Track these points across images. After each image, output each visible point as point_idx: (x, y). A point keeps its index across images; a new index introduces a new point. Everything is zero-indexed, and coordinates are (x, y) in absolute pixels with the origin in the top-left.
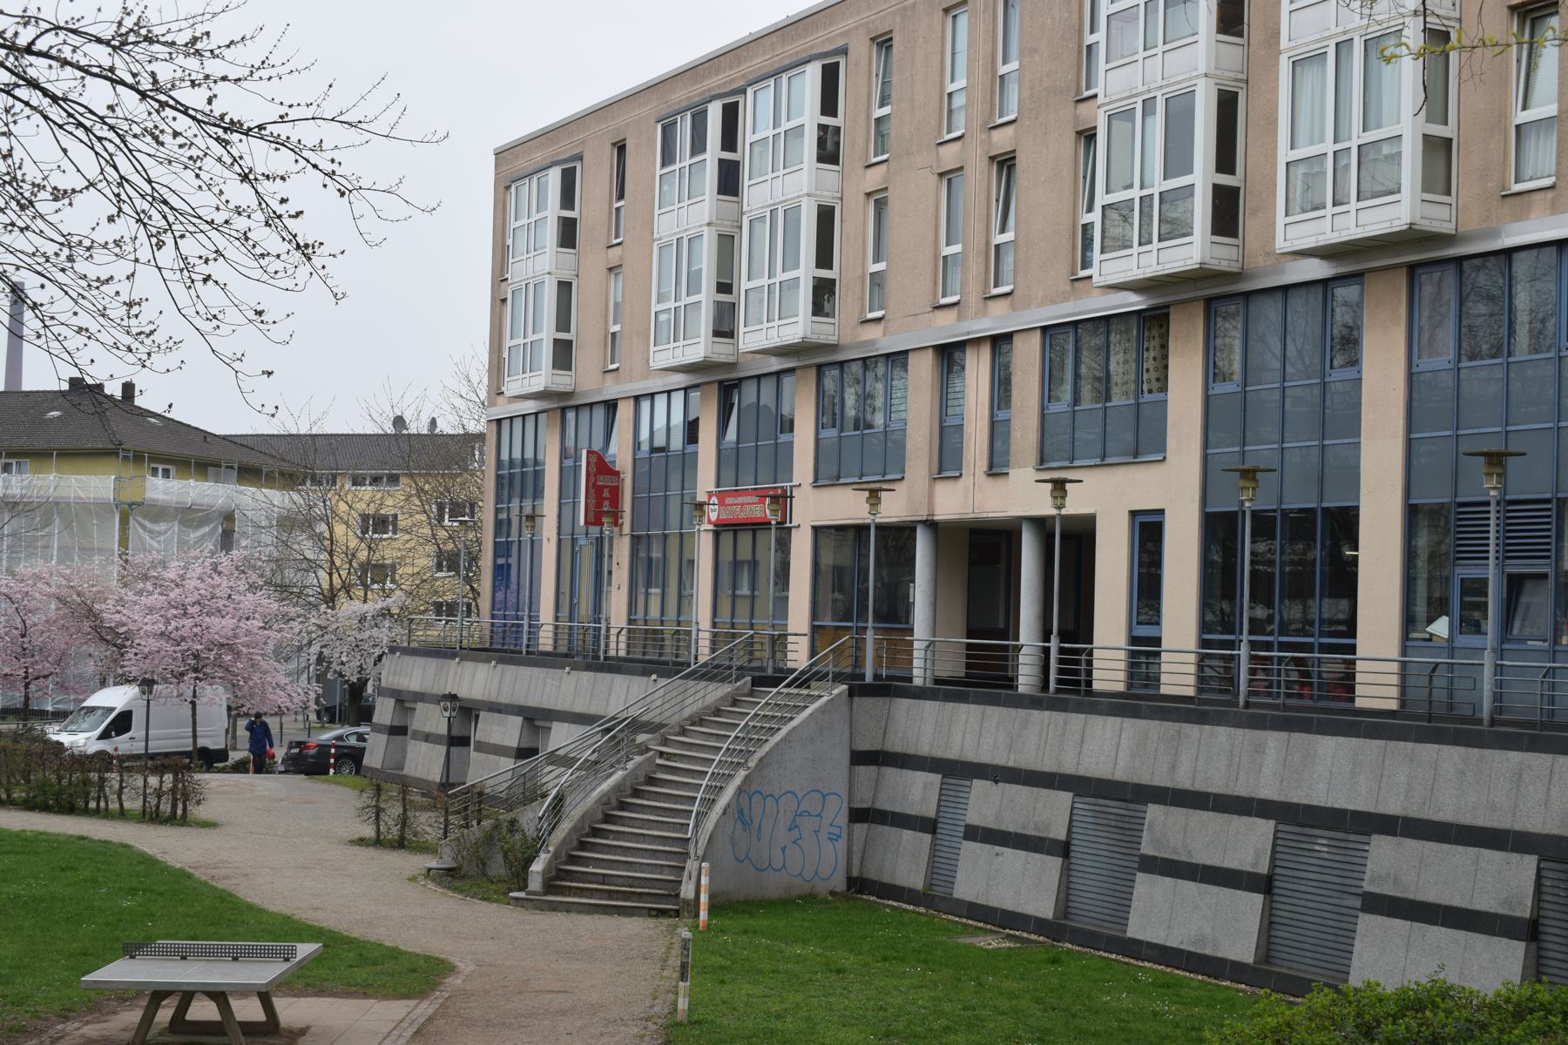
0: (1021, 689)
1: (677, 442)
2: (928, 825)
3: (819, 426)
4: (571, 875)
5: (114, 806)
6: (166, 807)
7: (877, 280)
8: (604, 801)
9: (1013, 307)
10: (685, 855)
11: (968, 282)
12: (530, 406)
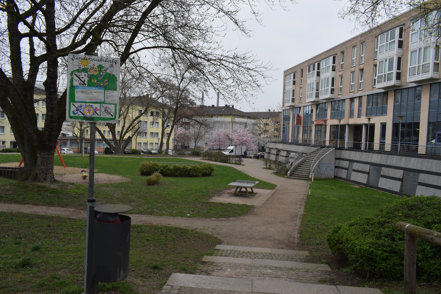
0: (362, 149)
1: (310, 113)
2: (347, 169)
3: (331, 110)
4: (293, 174)
5: (231, 162)
6: (238, 162)
7: (341, 88)
8: (298, 164)
10: (310, 172)
12: (288, 108)
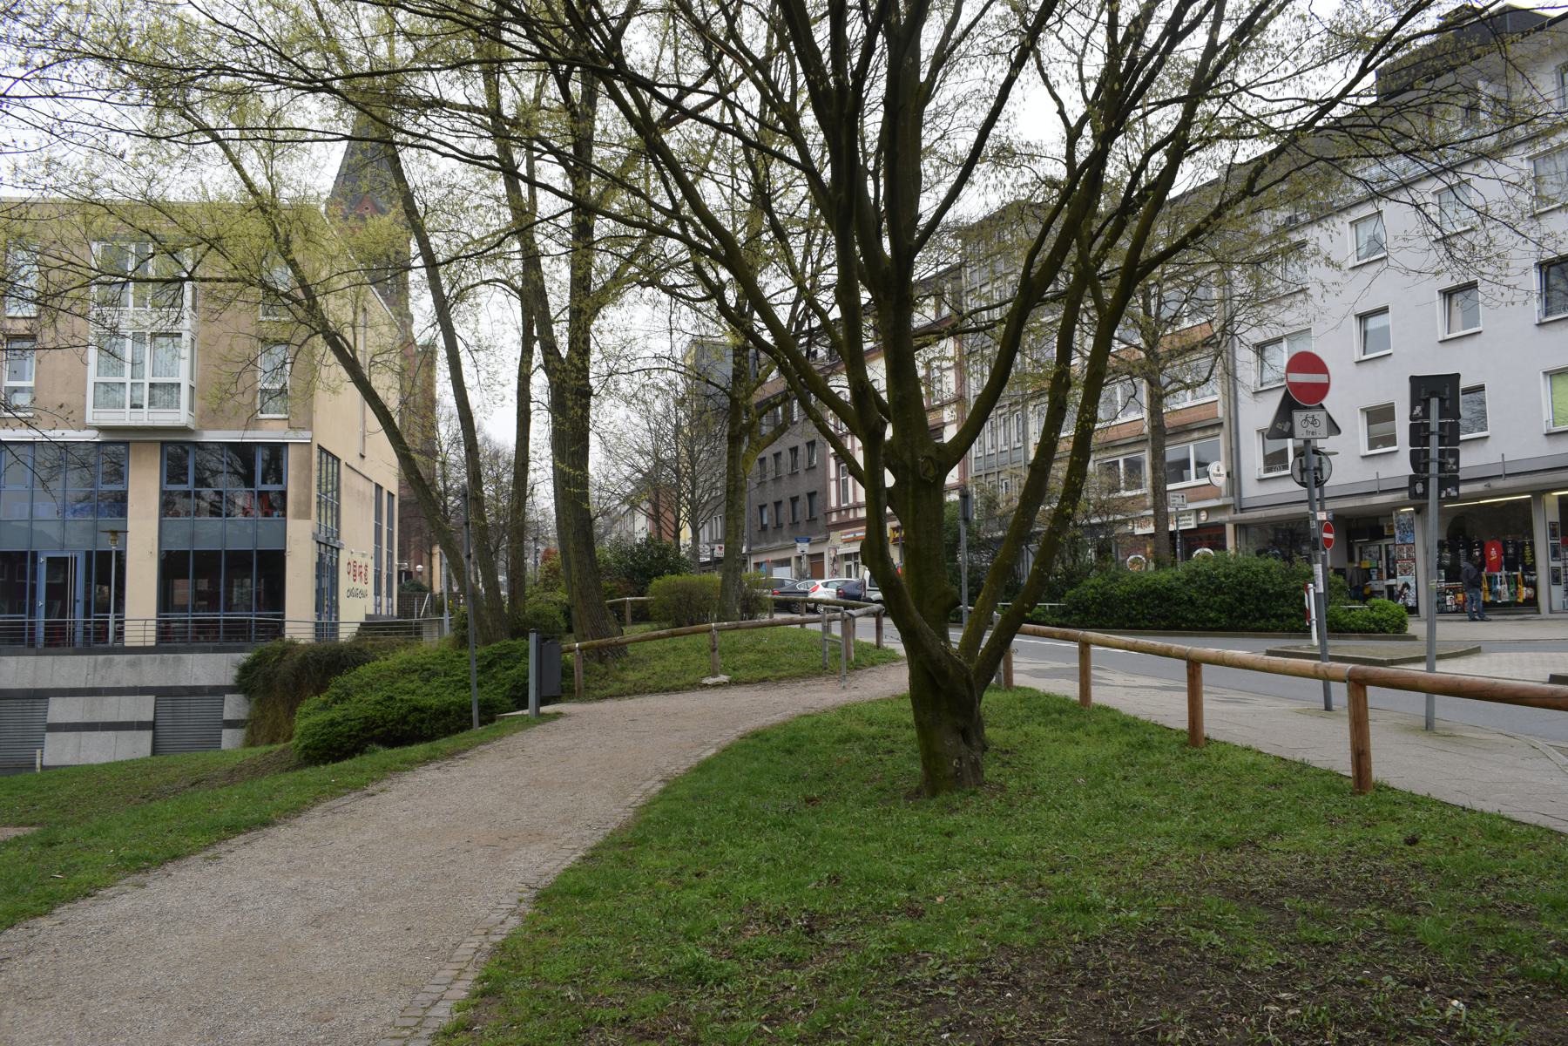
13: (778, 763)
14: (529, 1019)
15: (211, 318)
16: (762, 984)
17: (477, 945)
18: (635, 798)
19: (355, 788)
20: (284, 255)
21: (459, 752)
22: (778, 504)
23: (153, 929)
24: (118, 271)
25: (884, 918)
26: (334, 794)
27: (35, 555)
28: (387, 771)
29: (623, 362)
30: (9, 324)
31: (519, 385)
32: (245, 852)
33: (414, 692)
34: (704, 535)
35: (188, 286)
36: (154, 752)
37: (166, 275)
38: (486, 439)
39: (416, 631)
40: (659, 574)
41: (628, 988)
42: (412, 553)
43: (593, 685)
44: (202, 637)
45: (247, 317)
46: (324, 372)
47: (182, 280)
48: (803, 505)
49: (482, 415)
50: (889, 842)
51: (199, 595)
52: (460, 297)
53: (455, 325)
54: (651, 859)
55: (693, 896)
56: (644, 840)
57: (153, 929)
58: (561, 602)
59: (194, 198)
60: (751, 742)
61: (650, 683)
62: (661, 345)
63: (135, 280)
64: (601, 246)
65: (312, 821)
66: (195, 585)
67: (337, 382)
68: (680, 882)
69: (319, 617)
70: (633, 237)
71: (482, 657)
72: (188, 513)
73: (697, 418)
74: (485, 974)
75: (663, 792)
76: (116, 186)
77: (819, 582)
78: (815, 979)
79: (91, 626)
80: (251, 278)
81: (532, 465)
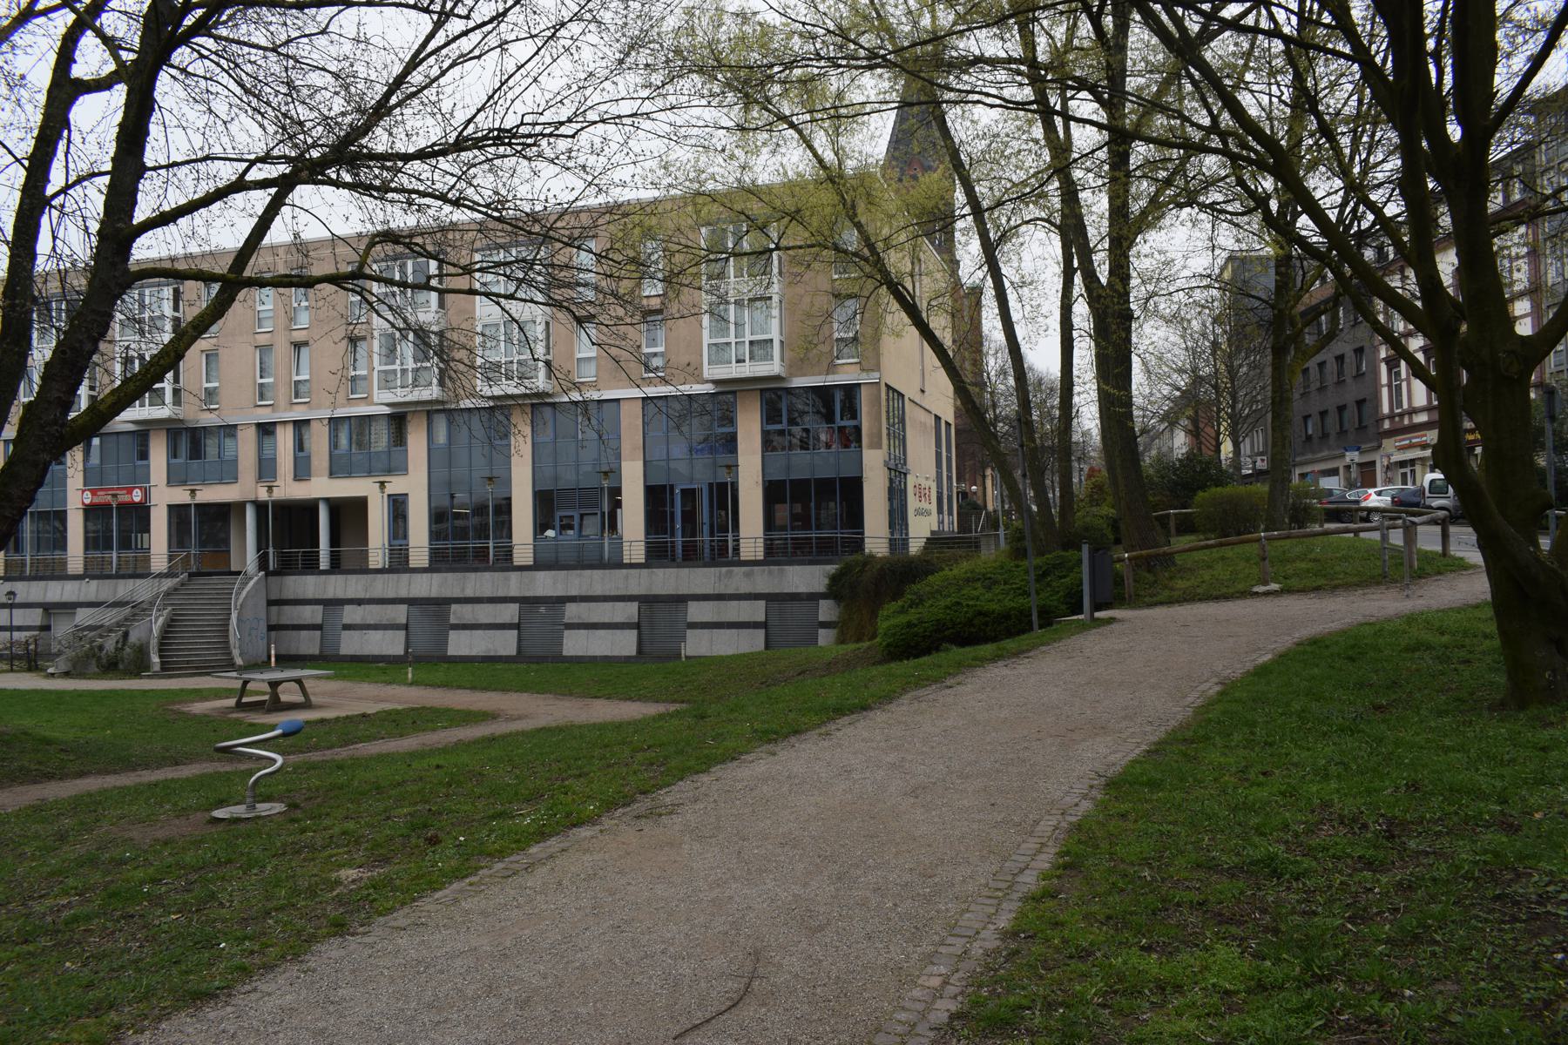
7: (210, 393)
9: (311, 409)
11: (283, 393)
13: (1341, 670)
14: (1110, 894)
15: (792, 280)
16: (1342, 883)
17: (1055, 823)
18: (1194, 698)
19: (936, 681)
20: (851, 220)
21: (1023, 652)
22: (1323, 414)
23: (785, 789)
24: (722, 248)
25: (1474, 830)
26: (918, 686)
27: (672, 487)
28: (961, 667)
29: (1163, 284)
30: (645, 302)
31: (1062, 315)
32: (849, 731)
33: (978, 599)
34: (1246, 448)
35: (775, 255)
36: (767, 646)
37: (758, 248)
38: (1030, 369)
39: (975, 545)
40: (1203, 487)
41: (1202, 874)
42: (967, 476)
43: (1142, 593)
44: (799, 552)
45: (826, 276)
46: (889, 318)
47: (772, 251)
48: (1351, 414)
49: (1028, 346)
50: (1473, 753)
51: (794, 517)
52: (1004, 237)
53: (1001, 265)
54: (1215, 756)
55: (1263, 794)
56: (1207, 738)
57: (785, 789)
58: (1107, 516)
59: (777, 179)
60: (1309, 649)
61: (1199, 591)
62: (1201, 263)
63: (735, 255)
64: (1138, 173)
65: (902, 708)
66: (791, 507)
67: (901, 327)
68: (1247, 780)
69: (892, 534)
70: (1170, 160)
71: (1037, 567)
72: (783, 449)
73: (1238, 337)
74: (1065, 849)
75: (1221, 693)
76: (718, 178)
77: (1371, 491)
78: (1400, 883)
79: (714, 544)
80: (827, 243)
81: (1076, 389)
